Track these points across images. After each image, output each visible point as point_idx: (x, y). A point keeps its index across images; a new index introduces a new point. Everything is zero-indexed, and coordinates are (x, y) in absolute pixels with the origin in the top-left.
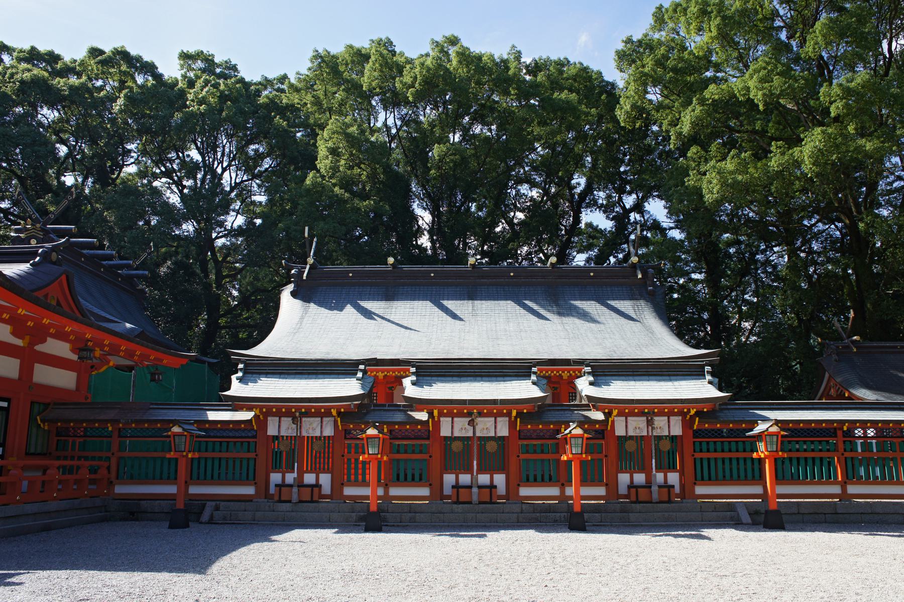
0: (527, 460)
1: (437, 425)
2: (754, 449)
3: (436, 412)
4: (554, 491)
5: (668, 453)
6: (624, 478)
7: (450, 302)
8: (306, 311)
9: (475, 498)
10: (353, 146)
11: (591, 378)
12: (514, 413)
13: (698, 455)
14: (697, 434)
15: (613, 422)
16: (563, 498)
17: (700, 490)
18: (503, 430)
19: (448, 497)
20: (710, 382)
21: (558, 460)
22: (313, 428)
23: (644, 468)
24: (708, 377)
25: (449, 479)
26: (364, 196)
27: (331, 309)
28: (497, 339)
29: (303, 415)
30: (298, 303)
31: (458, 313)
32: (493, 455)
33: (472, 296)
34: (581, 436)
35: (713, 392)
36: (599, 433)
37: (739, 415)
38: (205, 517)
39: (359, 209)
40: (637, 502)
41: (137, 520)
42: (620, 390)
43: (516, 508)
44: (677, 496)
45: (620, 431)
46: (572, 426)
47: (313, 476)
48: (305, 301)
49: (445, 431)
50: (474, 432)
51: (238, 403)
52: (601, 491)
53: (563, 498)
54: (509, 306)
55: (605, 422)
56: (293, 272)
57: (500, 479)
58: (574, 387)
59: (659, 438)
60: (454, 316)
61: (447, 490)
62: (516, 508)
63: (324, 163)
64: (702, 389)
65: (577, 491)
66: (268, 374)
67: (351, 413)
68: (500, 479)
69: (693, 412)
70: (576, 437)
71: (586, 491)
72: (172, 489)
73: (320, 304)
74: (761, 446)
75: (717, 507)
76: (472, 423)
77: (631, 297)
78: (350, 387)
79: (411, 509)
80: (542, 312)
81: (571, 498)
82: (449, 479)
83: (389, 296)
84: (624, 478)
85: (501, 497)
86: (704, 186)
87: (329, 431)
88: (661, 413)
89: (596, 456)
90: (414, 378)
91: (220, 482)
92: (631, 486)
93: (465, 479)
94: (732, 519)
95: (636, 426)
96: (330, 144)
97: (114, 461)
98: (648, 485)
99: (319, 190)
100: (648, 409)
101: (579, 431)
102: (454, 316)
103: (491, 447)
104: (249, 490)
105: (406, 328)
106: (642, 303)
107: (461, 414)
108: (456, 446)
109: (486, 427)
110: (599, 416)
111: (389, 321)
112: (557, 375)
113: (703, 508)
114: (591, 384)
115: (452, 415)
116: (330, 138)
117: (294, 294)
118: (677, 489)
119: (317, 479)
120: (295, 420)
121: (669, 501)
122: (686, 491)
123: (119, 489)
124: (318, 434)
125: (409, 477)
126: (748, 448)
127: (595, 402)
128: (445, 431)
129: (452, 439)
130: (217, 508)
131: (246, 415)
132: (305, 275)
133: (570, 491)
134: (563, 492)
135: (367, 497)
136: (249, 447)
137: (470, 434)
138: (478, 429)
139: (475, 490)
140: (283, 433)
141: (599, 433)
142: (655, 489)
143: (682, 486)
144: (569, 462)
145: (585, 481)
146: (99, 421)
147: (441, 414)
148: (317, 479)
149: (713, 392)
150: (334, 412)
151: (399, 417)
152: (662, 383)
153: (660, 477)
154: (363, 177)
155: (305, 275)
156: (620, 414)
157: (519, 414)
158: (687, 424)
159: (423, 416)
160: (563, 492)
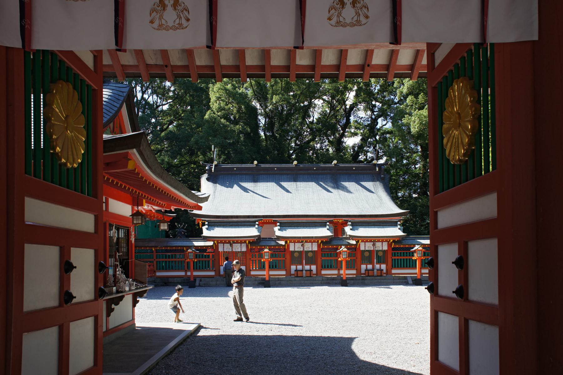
0: (325, 260)
1: (288, 246)
2: (413, 256)
3: (288, 242)
4: (335, 272)
5: (382, 257)
6: (363, 267)
7: (285, 183)
8: (215, 187)
9: (304, 275)
10: (230, 96)
11: (351, 227)
12: (320, 241)
13: (394, 258)
14: (394, 249)
15: (359, 245)
16: (339, 275)
17: (394, 271)
18: (315, 248)
19: (293, 275)
20: (399, 229)
21: (337, 260)
22: (237, 248)
23: (371, 263)
24: (399, 227)
25: (293, 268)
26: (236, 122)
27: (227, 187)
28: (309, 203)
29: (234, 243)
30: (210, 184)
31: (289, 189)
32: (311, 258)
33: (295, 180)
34: (346, 251)
35: (401, 233)
36: (353, 249)
37: (410, 242)
38: (197, 284)
39: (234, 131)
40: (368, 276)
41: (168, 285)
42: (362, 232)
43: (320, 279)
44: (384, 274)
45: (362, 248)
46: (343, 247)
47: (309, 266)
48: (214, 183)
49: (292, 249)
50: (303, 249)
51: (207, 239)
52: (354, 272)
53: (339, 275)
54: (313, 185)
55: (356, 245)
56: (207, 168)
57: (314, 268)
58: (344, 230)
59: (378, 251)
60: (288, 191)
62: (320, 279)
63: (214, 106)
64: (396, 232)
65: (344, 272)
66: (218, 226)
67: (255, 243)
68: (314, 268)
69: (391, 241)
70: (344, 251)
71: (348, 272)
72: (183, 273)
73: (222, 185)
74: (415, 254)
75: (400, 278)
76: (303, 245)
77: (373, 180)
79: (279, 280)
80: (329, 189)
81: (342, 275)
82: (293, 268)
83: (255, 180)
84: (363, 267)
85: (314, 275)
86: (411, 123)
88: (379, 241)
89: (352, 258)
90: (279, 227)
91: (176, 270)
92: (366, 270)
93: (300, 267)
94: (405, 282)
95: (369, 246)
96: (218, 95)
97: (155, 263)
98: (373, 270)
99: (213, 121)
100: (373, 240)
101: (346, 249)
102: (288, 191)
103: (310, 255)
104: (213, 273)
105: (266, 197)
106: (378, 183)
107: (298, 242)
108: (296, 255)
109: (308, 247)
110: (354, 242)
111: (257, 194)
112: (337, 223)
113: (394, 278)
114: (351, 229)
115: (295, 242)
116: (218, 92)
117: (208, 179)
118: (385, 271)
119: (310, 267)
120: (231, 245)
121: (381, 276)
122: (388, 272)
123: (159, 274)
124: (240, 250)
125: (326, 266)
126: (411, 255)
127: (352, 237)
128: (292, 249)
129: (295, 252)
130: (201, 281)
131: (210, 243)
132: (213, 169)
133: (342, 272)
134: (339, 272)
135: (264, 275)
136: (208, 257)
137: (302, 250)
138: (305, 247)
139: (304, 272)
141: (353, 249)
142: (375, 271)
143: (387, 270)
145: (348, 268)
146: (149, 247)
147: (290, 242)
148: (310, 267)
149: (401, 233)
150: (247, 242)
151: (273, 243)
152: (380, 229)
153: (377, 266)
154: (235, 111)
155: (213, 169)
156: (362, 241)
157: (322, 242)
158: (389, 245)
159: (283, 243)
160: (339, 272)
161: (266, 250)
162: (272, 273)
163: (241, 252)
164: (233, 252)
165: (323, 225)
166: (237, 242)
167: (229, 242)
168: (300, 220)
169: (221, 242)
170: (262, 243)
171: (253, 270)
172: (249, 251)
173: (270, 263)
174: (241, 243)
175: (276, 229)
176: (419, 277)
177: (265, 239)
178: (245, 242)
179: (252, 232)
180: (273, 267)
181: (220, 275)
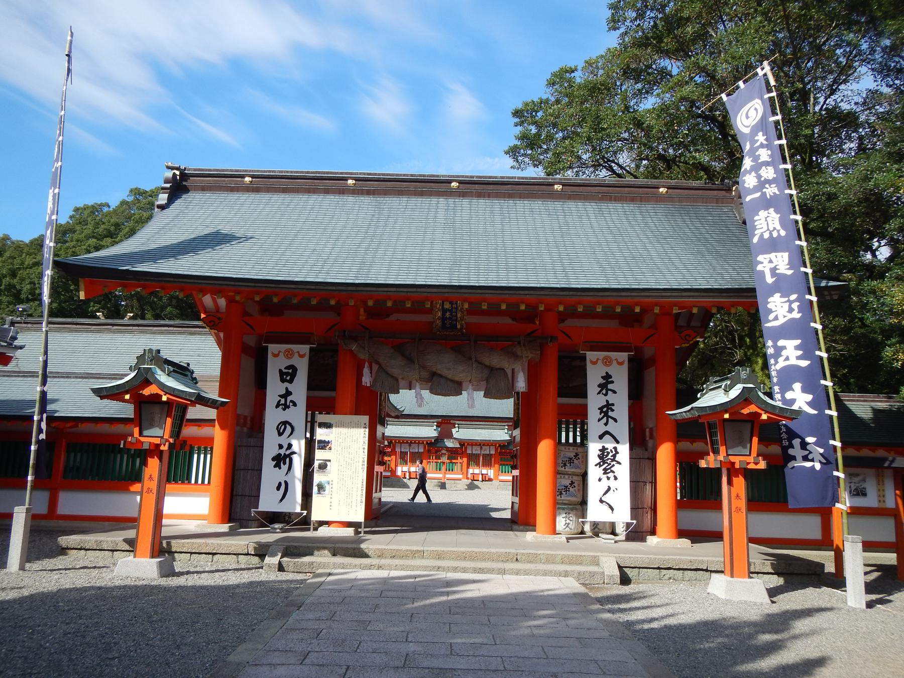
87: (421, 450)
163: (418, 453)
169: (399, 442)
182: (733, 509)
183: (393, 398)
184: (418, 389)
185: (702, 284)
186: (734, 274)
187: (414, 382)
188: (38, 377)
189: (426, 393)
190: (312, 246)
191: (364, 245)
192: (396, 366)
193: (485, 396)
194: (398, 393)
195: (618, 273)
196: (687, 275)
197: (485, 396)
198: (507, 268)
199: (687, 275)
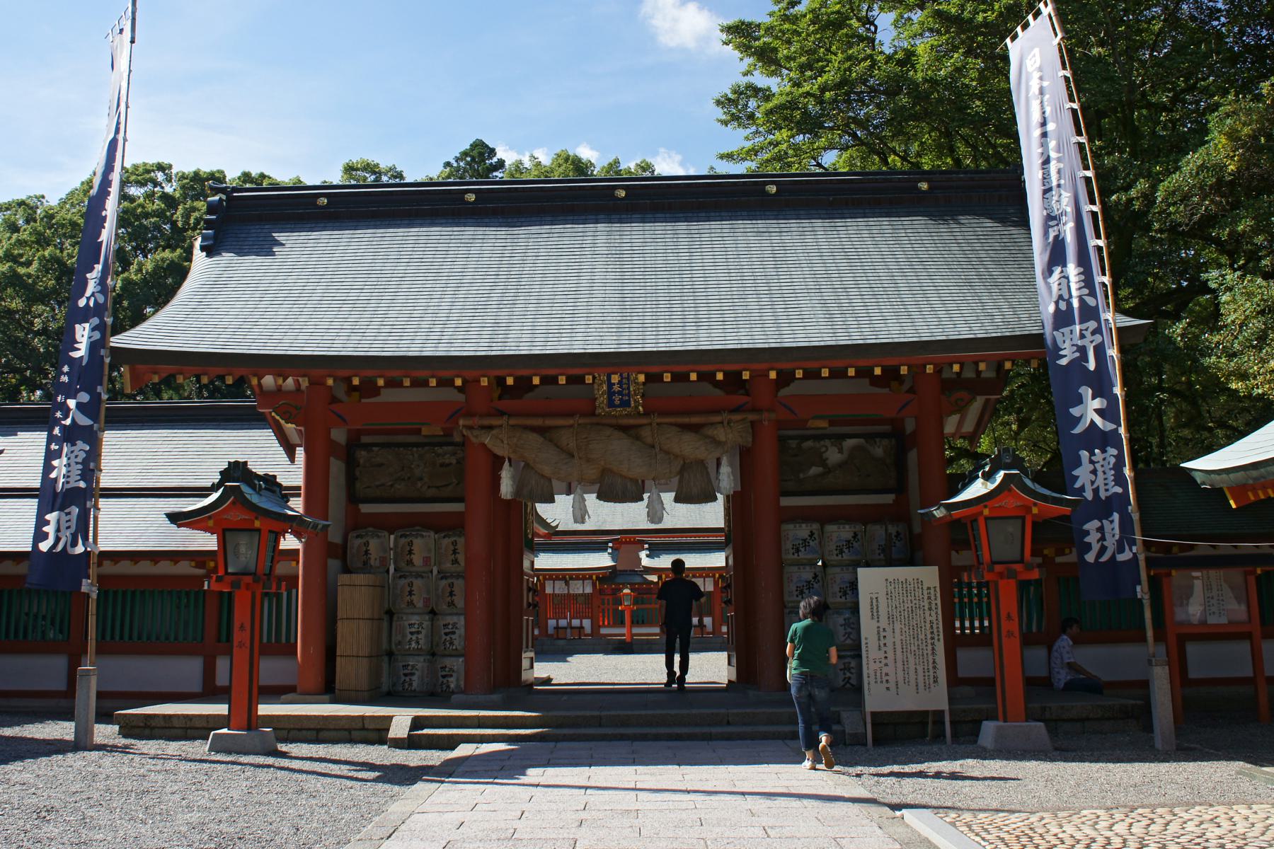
9: (569, 636)
18: (589, 590)
29: (571, 578)
61: (551, 631)
68: (587, 623)
78: (602, 560)
87: (589, 590)
93: (563, 623)
95: (558, 588)
109: (578, 588)
120: (567, 583)
140: (557, 592)
144: (622, 611)
147: (545, 579)
151: (638, 579)
157: (598, 578)
161: (626, 591)
162: (636, 630)
163: (583, 595)
164: (569, 595)
165: (600, 547)
166: (577, 578)
167: (564, 578)
168: (594, 538)
169: (551, 578)
170: (619, 580)
171: (604, 626)
172: (599, 592)
173: (632, 612)
174: (584, 579)
175: (643, 554)
176: (629, 640)
177: (624, 572)
178: (591, 577)
179: (602, 560)
180: (637, 622)
181: (547, 635)
182: (1004, 633)
183: (542, 509)
184: (654, 490)
185: (962, 331)
186: (1008, 313)
187: (573, 485)
188: (299, 495)
189: (591, 499)
190: (423, 302)
191: (495, 296)
192: (545, 458)
193: (677, 500)
194: (552, 501)
195: (851, 321)
196: (945, 321)
197: (677, 500)
198: (697, 323)
199: (945, 321)
